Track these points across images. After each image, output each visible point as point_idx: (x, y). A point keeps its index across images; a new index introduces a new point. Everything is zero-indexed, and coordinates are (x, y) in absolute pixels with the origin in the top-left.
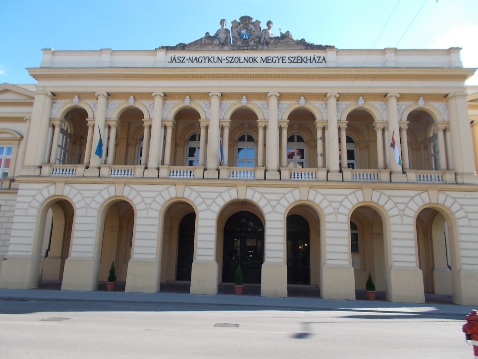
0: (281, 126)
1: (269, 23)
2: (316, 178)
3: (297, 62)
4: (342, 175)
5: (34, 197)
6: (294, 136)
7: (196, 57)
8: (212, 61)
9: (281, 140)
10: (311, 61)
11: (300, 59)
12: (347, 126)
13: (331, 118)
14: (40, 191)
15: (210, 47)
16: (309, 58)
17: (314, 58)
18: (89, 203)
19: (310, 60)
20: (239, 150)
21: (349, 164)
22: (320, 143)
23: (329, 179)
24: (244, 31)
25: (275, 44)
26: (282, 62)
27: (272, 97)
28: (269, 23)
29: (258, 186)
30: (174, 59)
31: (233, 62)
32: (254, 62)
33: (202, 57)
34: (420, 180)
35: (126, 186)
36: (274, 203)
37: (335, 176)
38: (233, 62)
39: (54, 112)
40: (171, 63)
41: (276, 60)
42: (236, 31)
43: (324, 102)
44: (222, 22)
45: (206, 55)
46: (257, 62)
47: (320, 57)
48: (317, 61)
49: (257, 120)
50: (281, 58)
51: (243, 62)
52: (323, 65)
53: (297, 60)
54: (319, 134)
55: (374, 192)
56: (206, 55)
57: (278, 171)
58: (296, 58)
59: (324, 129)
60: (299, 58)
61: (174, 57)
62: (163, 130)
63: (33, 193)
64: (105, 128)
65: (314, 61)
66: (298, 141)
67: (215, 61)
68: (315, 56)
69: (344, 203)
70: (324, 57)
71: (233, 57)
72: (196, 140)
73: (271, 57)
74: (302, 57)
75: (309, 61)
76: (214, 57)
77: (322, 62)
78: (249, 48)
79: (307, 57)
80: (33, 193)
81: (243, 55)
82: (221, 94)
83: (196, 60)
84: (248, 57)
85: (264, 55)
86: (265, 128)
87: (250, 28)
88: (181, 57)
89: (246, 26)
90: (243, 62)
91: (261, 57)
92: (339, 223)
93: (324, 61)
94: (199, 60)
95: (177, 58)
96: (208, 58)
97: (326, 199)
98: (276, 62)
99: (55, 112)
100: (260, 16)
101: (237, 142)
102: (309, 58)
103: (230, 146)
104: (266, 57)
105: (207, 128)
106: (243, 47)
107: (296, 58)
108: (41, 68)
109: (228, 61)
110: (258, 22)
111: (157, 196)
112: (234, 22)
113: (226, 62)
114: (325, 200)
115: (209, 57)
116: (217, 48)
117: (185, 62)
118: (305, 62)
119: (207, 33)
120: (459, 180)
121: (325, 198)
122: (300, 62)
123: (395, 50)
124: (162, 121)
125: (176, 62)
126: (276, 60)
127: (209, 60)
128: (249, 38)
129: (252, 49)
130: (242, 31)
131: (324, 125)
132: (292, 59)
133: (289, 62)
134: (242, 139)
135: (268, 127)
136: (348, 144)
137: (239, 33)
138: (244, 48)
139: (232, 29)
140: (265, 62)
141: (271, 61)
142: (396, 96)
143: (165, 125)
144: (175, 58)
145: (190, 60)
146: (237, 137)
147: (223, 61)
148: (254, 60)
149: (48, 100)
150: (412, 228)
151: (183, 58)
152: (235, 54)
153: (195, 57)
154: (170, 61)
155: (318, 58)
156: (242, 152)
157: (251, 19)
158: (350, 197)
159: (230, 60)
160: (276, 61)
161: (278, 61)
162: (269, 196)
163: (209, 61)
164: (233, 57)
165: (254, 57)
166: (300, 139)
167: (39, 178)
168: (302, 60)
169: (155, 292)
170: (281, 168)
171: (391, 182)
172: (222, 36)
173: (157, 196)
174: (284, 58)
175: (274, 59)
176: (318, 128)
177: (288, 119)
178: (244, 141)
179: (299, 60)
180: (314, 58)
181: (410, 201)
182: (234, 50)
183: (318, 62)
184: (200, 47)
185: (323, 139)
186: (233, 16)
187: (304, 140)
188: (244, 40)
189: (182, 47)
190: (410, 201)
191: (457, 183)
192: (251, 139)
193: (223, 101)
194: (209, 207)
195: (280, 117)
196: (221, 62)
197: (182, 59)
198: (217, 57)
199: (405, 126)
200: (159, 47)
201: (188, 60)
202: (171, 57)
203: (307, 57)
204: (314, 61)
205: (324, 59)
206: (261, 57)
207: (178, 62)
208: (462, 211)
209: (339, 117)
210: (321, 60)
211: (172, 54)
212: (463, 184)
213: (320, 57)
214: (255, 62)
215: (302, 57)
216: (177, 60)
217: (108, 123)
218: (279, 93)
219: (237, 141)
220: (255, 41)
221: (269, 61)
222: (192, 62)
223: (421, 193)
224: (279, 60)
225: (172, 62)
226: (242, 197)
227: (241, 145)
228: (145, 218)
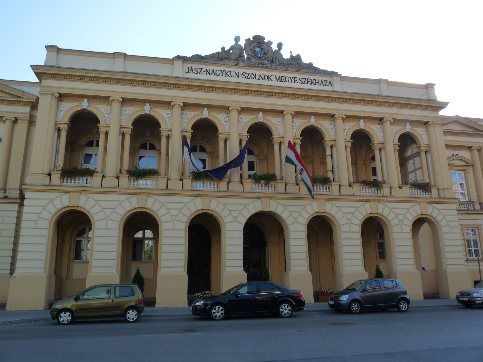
0: (241, 139)
1: (280, 45)
2: (275, 190)
3: (307, 83)
4: (243, 185)
5: (44, 207)
6: (197, 145)
7: (213, 70)
8: (229, 75)
9: (225, 151)
10: (319, 84)
11: (310, 81)
12: (301, 142)
13: (338, 136)
14: (186, 204)
15: (227, 61)
16: (317, 81)
17: (322, 81)
18: (234, 215)
19: (319, 82)
20: (140, 158)
21: (250, 176)
22: (329, 159)
23: (230, 189)
24: (258, 50)
25: (288, 65)
26: (295, 83)
27: (176, 106)
28: (280, 45)
29: (158, 194)
30: (192, 69)
31: (249, 78)
32: (269, 80)
33: (219, 71)
34: (412, 194)
35: (148, 197)
36: (295, 215)
37: (175, 184)
38: (249, 78)
39: (61, 115)
40: (188, 73)
41: (219, 73)
42: (250, 48)
43: (227, 115)
44: (237, 39)
45: (223, 69)
46: (272, 80)
47: (327, 81)
48: (324, 84)
49: (160, 129)
50: (293, 79)
51: (258, 79)
52: (329, 88)
53: (308, 81)
54: (328, 152)
55: (271, 201)
56: (223, 69)
57: (181, 180)
58: (306, 80)
59: (226, 141)
60: (309, 80)
61: (192, 68)
62: (56, 133)
63: (180, 206)
64: (120, 135)
65: (191, 71)
66: (150, 149)
67: (232, 75)
68: (192, 66)
69: (183, 211)
70: (330, 82)
71: (249, 73)
72: (93, 146)
73: (284, 77)
74: (311, 79)
75: (317, 84)
76: (231, 72)
77: (329, 86)
78: (263, 66)
79: (316, 80)
80: (180, 206)
81: (259, 72)
82: (123, 99)
83: (214, 72)
84: (263, 75)
85: (278, 74)
86: (168, 137)
87: (264, 47)
88: (198, 68)
89: (259, 45)
90: (258, 79)
91: (275, 76)
92: (352, 232)
93: (330, 85)
94: (217, 73)
95: (194, 69)
96: (225, 72)
97: (393, 211)
98: (219, 75)
99: (61, 115)
100: (272, 37)
101: (138, 150)
102: (317, 81)
103: (131, 154)
104: (280, 76)
105: (107, 133)
106: (258, 64)
107: (306, 80)
108: (45, 66)
109: (244, 77)
110: (270, 43)
111: (183, 208)
112: (248, 40)
113: (243, 78)
114: (163, 208)
115: (226, 71)
116: (234, 63)
117: (202, 74)
118: (314, 84)
119: (223, 48)
120: (442, 195)
121: (391, 210)
122: (310, 84)
123: (125, 56)
124: (56, 123)
125: (193, 73)
126: (219, 73)
127: (226, 74)
128: (263, 57)
129: (266, 68)
130: (256, 49)
131: (281, 140)
132: (303, 81)
133: (300, 83)
134: (143, 147)
135: (171, 136)
136: (248, 155)
137: (254, 52)
138: (260, 65)
139: (245, 45)
140: (279, 80)
141: (285, 80)
142: (390, 121)
143: (123, 132)
144: (192, 69)
145: (207, 72)
146: (137, 146)
147: (239, 76)
148: (269, 78)
149: (54, 101)
150: (241, 234)
151: (200, 69)
152: (251, 71)
153: (212, 70)
154: (187, 72)
155: (325, 82)
156: (143, 159)
157: (264, 39)
158: (360, 209)
159: (246, 75)
160: (289, 80)
161: (221, 75)
162: (291, 209)
163: (226, 75)
164: (249, 73)
165: (269, 75)
166: (203, 150)
167: (48, 188)
168: (312, 82)
169: (43, 309)
170: (183, 177)
171: (391, 195)
172: (237, 52)
173: (355, 212)
174: (296, 79)
175: (287, 79)
176: (162, 136)
177: (301, 137)
178: (146, 148)
179: (309, 82)
180: (322, 81)
181: (243, 208)
182: (249, 66)
183: (325, 85)
184: (217, 60)
185: (332, 156)
186: (246, 34)
187: (207, 151)
188: (259, 58)
189: (198, 58)
190: (243, 208)
191: (440, 198)
192: (152, 147)
193: (61, 103)
194: (235, 218)
195: (241, 131)
196: (238, 77)
197: (199, 71)
198: (234, 72)
199: (349, 145)
200: (175, 56)
201: (205, 72)
202: (188, 67)
203: (316, 80)
204: (322, 84)
205: (330, 83)
206: (275, 76)
207: (195, 73)
208: (444, 220)
209: (294, 134)
210: (328, 84)
211: (190, 65)
212: (444, 198)
213: (327, 81)
214: (270, 79)
215: (311, 79)
216: (194, 71)
217: (59, 126)
218: (182, 102)
219: (139, 148)
220: (269, 60)
221: (283, 80)
222: (209, 74)
223: (414, 205)
224: (291, 80)
225: (190, 73)
226: (266, 209)
227: (142, 152)
228: (172, 230)
